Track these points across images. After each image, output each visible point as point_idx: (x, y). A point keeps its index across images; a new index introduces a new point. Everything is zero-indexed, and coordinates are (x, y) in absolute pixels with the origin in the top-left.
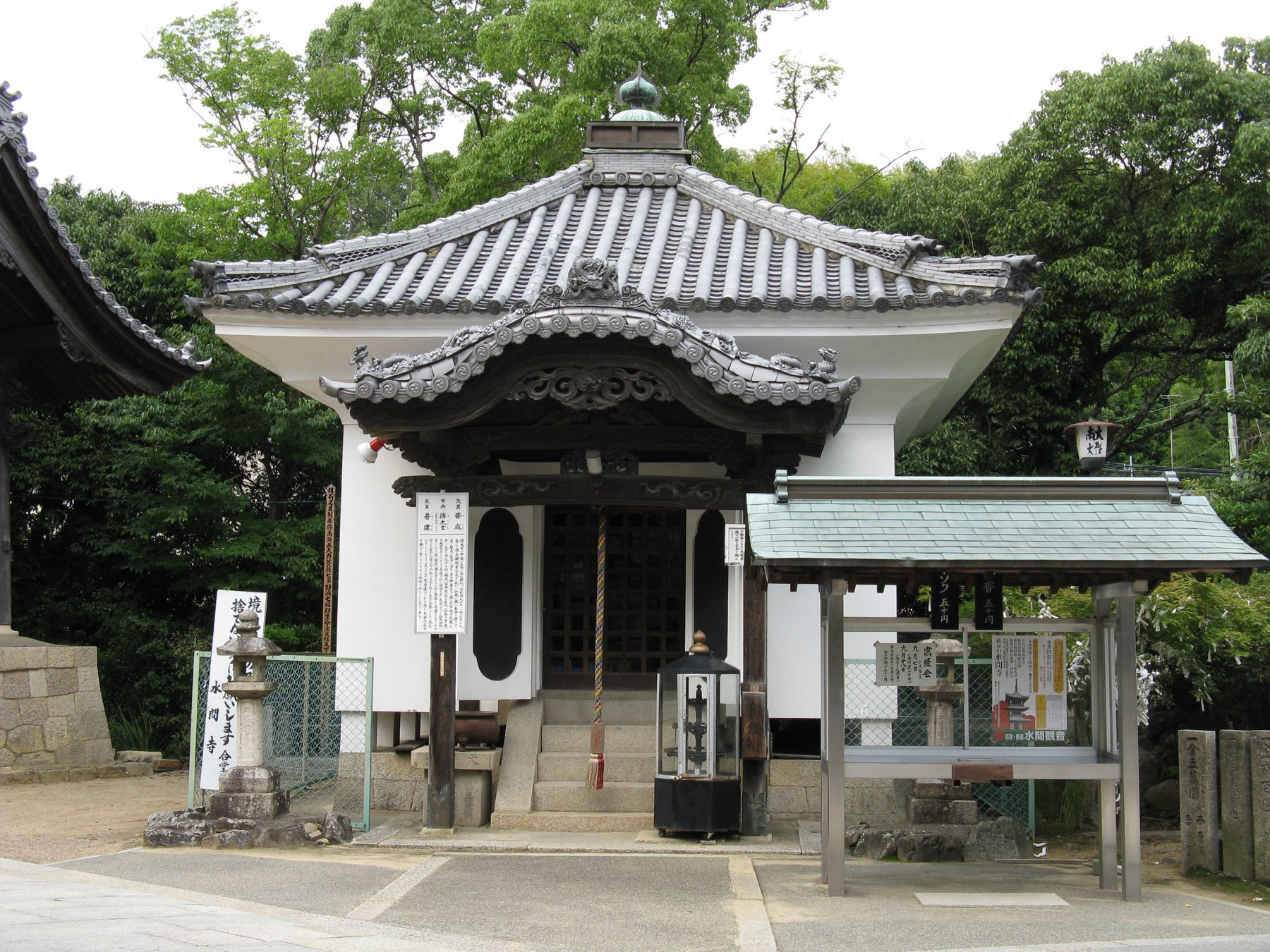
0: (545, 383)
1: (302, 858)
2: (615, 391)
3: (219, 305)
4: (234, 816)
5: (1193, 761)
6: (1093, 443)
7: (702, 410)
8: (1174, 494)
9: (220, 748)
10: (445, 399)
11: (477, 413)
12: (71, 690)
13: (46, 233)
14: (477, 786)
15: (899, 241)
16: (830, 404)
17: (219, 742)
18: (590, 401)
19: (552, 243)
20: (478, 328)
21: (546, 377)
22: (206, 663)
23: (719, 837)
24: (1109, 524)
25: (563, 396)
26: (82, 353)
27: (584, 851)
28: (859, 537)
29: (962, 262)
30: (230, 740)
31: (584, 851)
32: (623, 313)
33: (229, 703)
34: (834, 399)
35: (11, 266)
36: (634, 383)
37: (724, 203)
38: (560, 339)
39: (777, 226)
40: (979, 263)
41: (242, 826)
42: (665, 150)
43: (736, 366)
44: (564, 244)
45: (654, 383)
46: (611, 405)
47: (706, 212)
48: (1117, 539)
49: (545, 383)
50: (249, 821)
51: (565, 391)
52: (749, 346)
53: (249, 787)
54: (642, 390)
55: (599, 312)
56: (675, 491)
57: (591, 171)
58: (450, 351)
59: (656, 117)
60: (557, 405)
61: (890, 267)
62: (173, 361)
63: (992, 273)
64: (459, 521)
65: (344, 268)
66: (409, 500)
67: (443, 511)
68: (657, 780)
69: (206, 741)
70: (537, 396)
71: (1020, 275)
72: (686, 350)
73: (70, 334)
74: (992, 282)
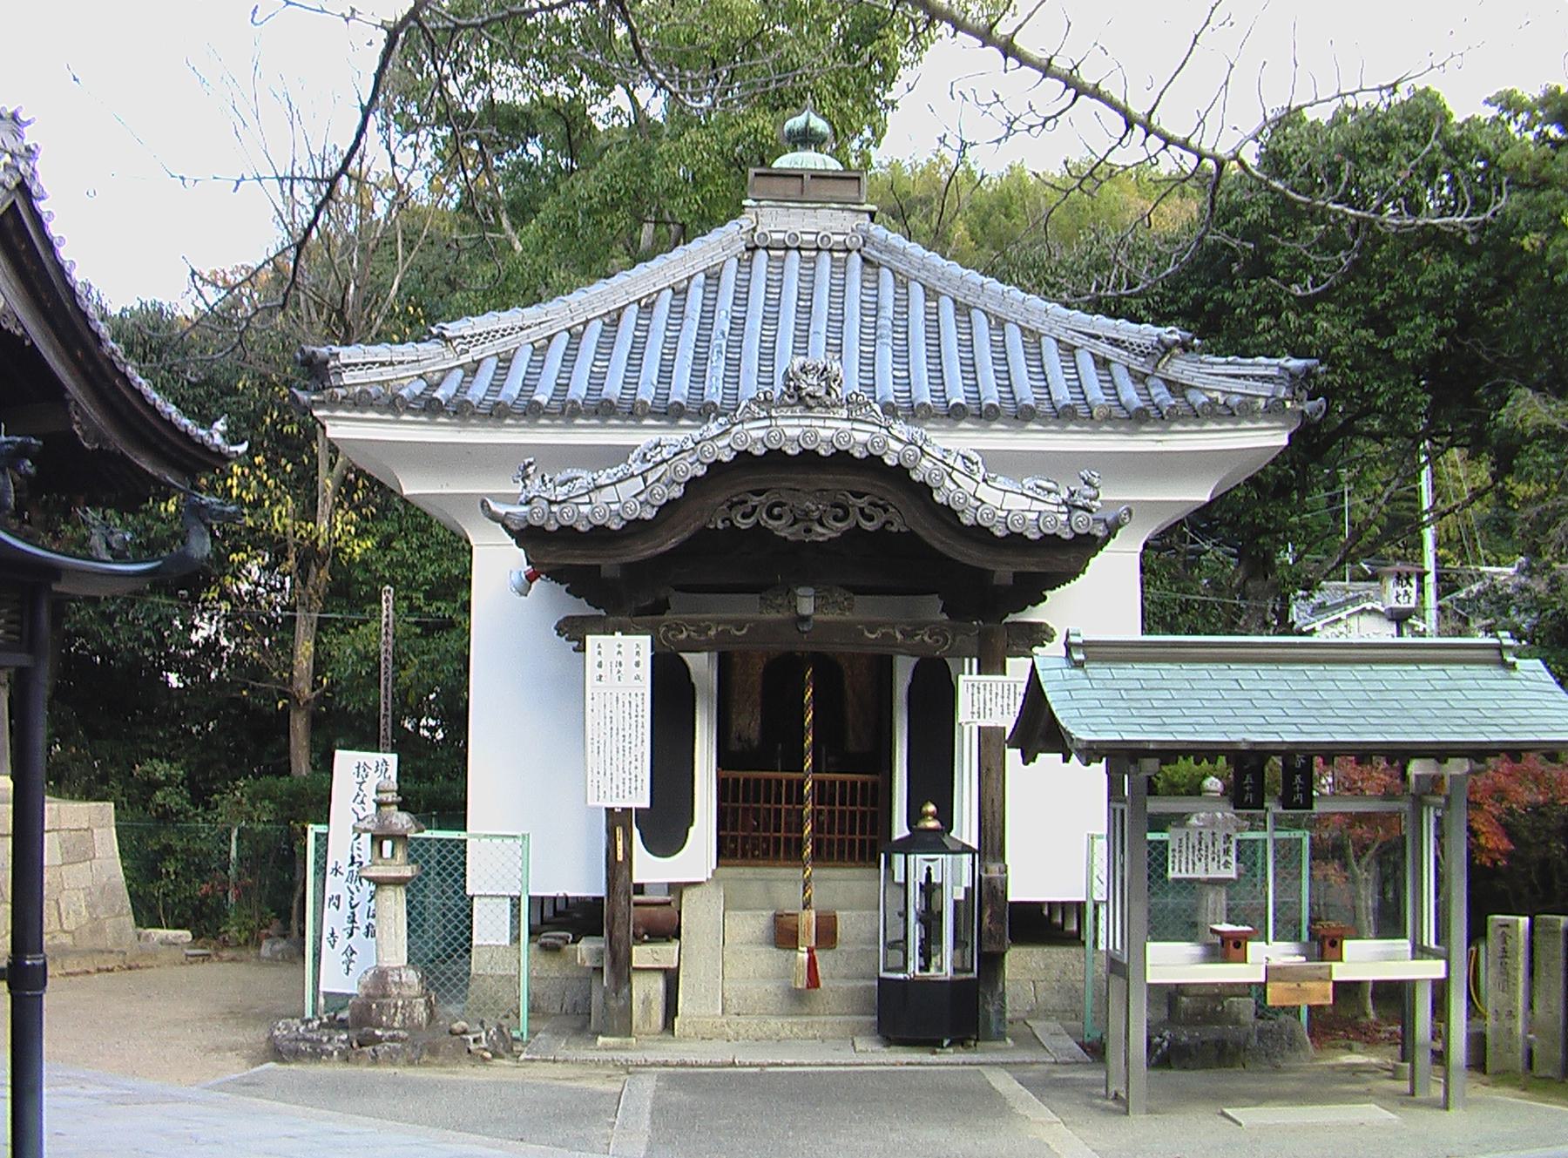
0: (754, 508)
1: (468, 1074)
2: (836, 519)
3: (333, 403)
4: (379, 1026)
5: (1504, 951)
6: (1401, 591)
7: (938, 540)
8: (1510, 659)
9: (343, 941)
10: (636, 527)
11: (671, 544)
12: (87, 856)
13: (61, 290)
14: (658, 984)
15: (1147, 333)
16: (1095, 537)
17: (342, 935)
18: (808, 531)
19: (723, 323)
20: (675, 437)
21: (755, 500)
22: (322, 839)
23: (960, 1042)
24: (1445, 695)
25: (776, 523)
26: (97, 440)
27: (802, 1065)
28: (1177, 712)
29: (1228, 363)
30: (356, 934)
31: (802, 1065)
32: (848, 425)
33: (353, 889)
34: (1099, 531)
35: (19, 332)
36: (862, 510)
37: (923, 274)
38: (775, 458)
39: (992, 307)
40: (1249, 366)
41: (393, 1039)
42: (844, 204)
43: (983, 492)
44: (738, 324)
45: (886, 510)
46: (834, 535)
47: (902, 283)
48: (1461, 713)
49: (754, 508)
50: (402, 1034)
51: (779, 517)
52: (999, 463)
53: (395, 991)
54: (870, 519)
55: (821, 423)
56: (899, 636)
57: (754, 229)
58: (637, 468)
59: (1425, 474)
60: (769, 532)
61: (1137, 364)
62: (203, 447)
63: (1263, 378)
64: (638, 671)
65: (474, 353)
66: (575, 644)
67: (619, 658)
68: (881, 980)
69: (326, 934)
70: (744, 524)
71: (1301, 382)
72: (923, 470)
73: (85, 416)
74: (1266, 390)
